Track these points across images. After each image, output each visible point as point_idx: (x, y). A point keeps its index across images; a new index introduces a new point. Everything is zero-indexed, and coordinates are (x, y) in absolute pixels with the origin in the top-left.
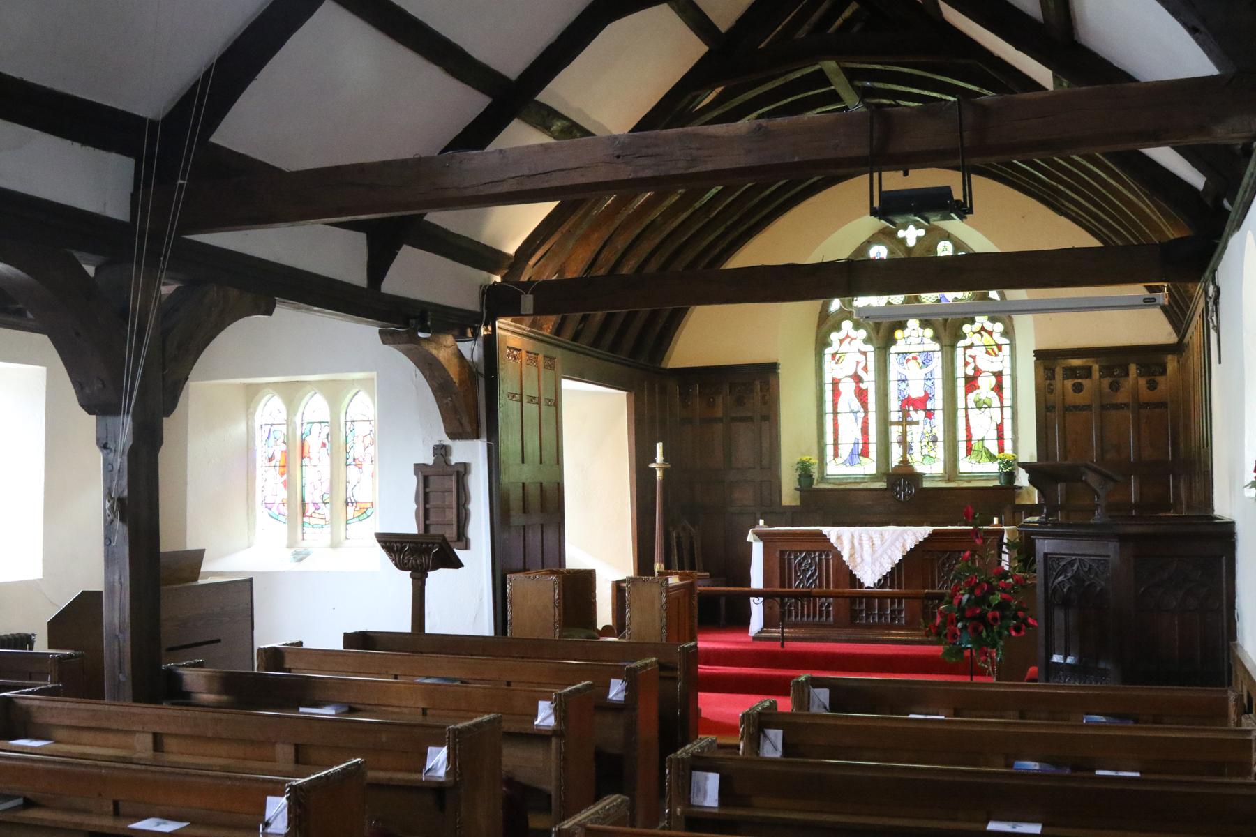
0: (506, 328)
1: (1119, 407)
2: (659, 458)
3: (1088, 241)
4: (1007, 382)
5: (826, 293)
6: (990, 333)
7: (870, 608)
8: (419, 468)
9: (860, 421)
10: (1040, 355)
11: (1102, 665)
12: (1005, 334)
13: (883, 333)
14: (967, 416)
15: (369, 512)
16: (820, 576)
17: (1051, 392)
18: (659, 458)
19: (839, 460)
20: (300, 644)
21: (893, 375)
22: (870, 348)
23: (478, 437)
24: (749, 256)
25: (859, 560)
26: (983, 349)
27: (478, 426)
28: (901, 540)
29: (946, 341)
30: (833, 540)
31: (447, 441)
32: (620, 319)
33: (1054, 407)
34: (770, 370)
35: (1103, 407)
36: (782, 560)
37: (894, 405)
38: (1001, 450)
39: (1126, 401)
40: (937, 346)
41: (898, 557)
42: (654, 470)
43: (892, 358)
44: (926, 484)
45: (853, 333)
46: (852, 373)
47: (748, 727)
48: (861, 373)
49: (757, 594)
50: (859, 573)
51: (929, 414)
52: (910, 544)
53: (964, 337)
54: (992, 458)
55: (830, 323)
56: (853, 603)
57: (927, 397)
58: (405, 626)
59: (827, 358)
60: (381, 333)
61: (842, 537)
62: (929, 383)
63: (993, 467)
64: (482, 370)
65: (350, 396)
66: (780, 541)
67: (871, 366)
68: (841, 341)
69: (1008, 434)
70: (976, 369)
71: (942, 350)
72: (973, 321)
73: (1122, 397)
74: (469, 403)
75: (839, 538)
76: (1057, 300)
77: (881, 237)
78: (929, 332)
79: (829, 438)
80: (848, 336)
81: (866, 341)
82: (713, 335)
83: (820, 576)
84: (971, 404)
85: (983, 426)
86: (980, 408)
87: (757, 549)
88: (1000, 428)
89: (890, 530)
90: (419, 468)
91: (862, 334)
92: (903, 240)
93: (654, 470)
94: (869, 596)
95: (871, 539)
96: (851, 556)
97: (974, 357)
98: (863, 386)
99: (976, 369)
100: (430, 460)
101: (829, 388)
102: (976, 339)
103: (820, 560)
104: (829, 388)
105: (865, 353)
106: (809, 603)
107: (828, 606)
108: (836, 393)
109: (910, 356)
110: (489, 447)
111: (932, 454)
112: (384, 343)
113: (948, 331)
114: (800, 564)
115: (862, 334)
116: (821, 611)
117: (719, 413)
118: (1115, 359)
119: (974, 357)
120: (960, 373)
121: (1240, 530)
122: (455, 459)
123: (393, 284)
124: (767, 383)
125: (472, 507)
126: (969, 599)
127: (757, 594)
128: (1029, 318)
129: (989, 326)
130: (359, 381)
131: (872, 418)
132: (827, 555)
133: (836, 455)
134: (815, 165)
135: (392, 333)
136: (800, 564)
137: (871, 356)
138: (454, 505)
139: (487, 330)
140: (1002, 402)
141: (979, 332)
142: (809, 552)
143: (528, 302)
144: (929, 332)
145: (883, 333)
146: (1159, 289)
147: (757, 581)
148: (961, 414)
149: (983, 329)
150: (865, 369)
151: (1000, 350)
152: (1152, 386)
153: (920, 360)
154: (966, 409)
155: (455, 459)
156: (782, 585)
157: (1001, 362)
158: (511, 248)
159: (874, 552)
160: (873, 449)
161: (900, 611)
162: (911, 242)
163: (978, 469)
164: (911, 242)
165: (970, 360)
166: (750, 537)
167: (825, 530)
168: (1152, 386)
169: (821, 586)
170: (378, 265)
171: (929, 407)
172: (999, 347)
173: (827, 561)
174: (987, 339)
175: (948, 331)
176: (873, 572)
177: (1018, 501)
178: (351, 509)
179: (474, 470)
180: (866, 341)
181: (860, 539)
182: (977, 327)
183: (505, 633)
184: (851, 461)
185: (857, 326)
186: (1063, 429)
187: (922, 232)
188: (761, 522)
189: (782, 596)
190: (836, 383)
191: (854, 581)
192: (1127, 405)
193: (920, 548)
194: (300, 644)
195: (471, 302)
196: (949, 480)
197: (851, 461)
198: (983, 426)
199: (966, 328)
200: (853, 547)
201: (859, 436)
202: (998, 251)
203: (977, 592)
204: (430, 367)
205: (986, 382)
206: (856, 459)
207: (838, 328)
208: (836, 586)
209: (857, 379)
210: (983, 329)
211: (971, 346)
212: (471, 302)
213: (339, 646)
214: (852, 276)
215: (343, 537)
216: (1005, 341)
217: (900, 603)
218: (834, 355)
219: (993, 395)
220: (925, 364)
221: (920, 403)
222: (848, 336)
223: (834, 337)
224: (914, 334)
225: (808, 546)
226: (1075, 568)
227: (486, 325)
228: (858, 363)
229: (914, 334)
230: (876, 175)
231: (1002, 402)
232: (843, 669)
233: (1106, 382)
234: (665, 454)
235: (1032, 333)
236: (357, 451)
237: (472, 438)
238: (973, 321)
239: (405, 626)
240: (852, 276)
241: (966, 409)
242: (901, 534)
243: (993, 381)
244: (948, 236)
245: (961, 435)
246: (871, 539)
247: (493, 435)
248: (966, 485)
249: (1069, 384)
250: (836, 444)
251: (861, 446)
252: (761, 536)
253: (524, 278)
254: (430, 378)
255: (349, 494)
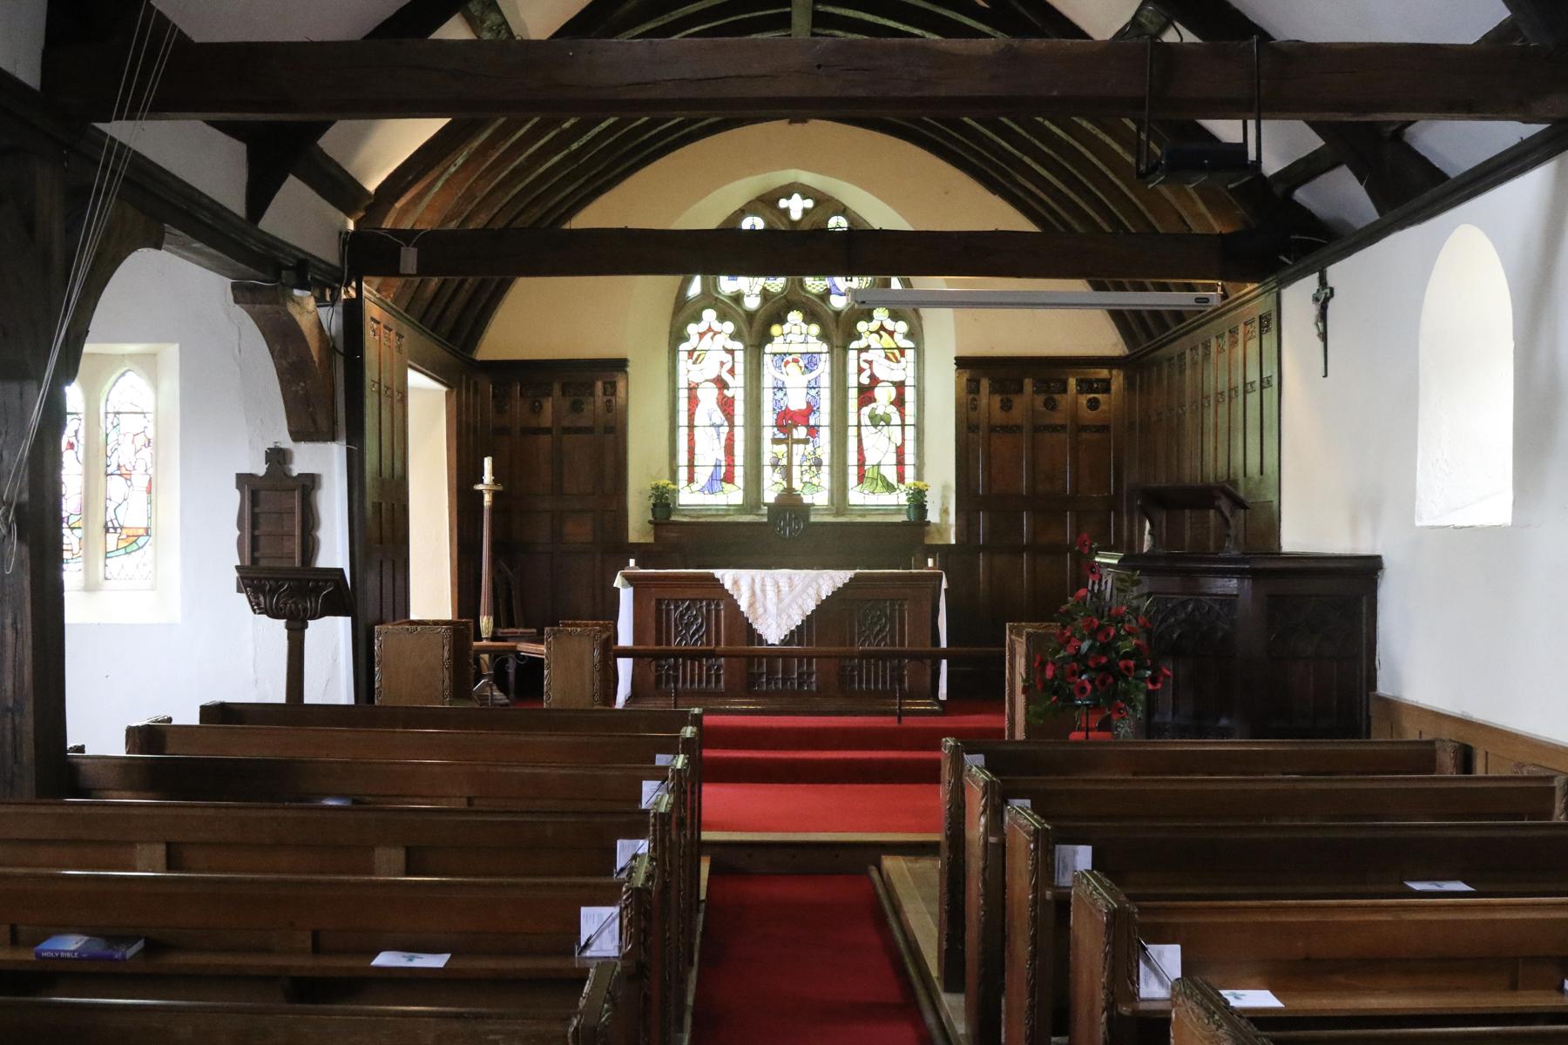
0: (372, 296)
1: (1054, 429)
2: (488, 477)
3: (1020, 223)
4: (910, 394)
5: (686, 270)
6: (891, 334)
7: (771, 672)
8: (243, 480)
9: (723, 437)
10: (962, 363)
11: (1224, 722)
12: (909, 335)
13: (755, 331)
14: (859, 435)
15: (141, 541)
16: (708, 631)
17: (975, 408)
18: (488, 477)
19: (695, 487)
20: (170, 720)
21: (767, 382)
22: (738, 345)
23: (333, 439)
24: (595, 216)
25: (760, 611)
26: (882, 353)
27: (334, 422)
28: (815, 586)
29: (838, 341)
30: (727, 586)
31: (286, 442)
32: (454, 286)
33: (977, 427)
34: (619, 365)
35: (1037, 429)
36: (659, 610)
37: (768, 418)
38: (901, 479)
39: (1061, 422)
40: (825, 347)
41: (811, 606)
42: (481, 493)
43: (767, 359)
44: (813, 519)
45: (716, 326)
46: (714, 376)
47: (993, 798)
48: (727, 377)
49: (625, 653)
50: (760, 627)
51: (813, 431)
52: (826, 591)
53: (859, 337)
54: (890, 488)
55: (688, 311)
56: (750, 664)
57: (811, 409)
58: (278, 695)
59: (683, 356)
60: (234, 287)
61: (739, 582)
62: (813, 392)
63: (901, 498)
64: (340, 346)
65: (114, 378)
66: (656, 586)
67: (740, 369)
68: (702, 335)
69: (910, 458)
70: (873, 377)
71: (831, 352)
72: (870, 318)
73: (1058, 418)
74: (329, 392)
75: (735, 583)
76: (1057, 294)
77: (760, 206)
78: (815, 329)
79: (683, 458)
80: (710, 329)
81: (733, 337)
82: (541, 318)
83: (708, 631)
84: (865, 420)
85: (879, 447)
86: (875, 426)
87: (626, 596)
88: (900, 451)
89: (800, 576)
90: (243, 480)
91: (729, 327)
92: (786, 211)
93: (481, 493)
94: (773, 655)
95: (777, 584)
96: (751, 605)
97: (870, 363)
98: (728, 393)
99: (873, 377)
100: (260, 469)
101: (683, 395)
102: (873, 340)
103: (708, 611)
104: (683, 395)
105: (731, 352)
106: (693, 665)
107: (718, 669)
108: (693, 401)
109: (789, 358)
110: (350, 453)
111: (815, 481)
112: (236, 301)
113: (840, 331)
114: (682, 615)
115: (729, 327)
116: (709, 676)
117: (546, 419)
118: (1048, 371)
119: (870, 363)
120: (852, 381)
121: (1386, 562)
122: (297, 468)
123: (270, 223)
124: (614, 385)
125: (323, 534)
126: (1091, 648)
127: (625, 653)
128: (948, 313)
129: (889, 325)
130: (131, 356)
131: (739, 434)
132: (718, 605)
133: (691, 479)
134: (710, 104)
135: (253, 289)
136: (682, 615)
137: (740, 356)
138: (297, 532)
139: (347, 292)
140: (903, 420)
141: (877, 332)
142: (693, 601)
143: (409, 258)
144: (815, 329)
145: (755, 331)
146: (1212, 288)
147: (625, 638)
148: (852, 432)
149: (882, 328)
150: (732, 371)
151: (902, 355)
152: (1006, 406)
153: (802, 363)
154: (859, 426)
155: (297, 468)
156: (659, 643)
157: (905, 370)
158: (372, 186)
159: (780, 600)
160: (739, 472)
161: (810, 675)
162: (796, 215)
163: (874, 501)
164: (796, 215)
165: (865, 366)
166: (618, 582)
167: (718, 573)
168: (1051, 405)
169: (709, 643)
170: (260, 193)
171: (812, 422)
172: (902, 351)
173: (718, 612)
174: (886, 341)
175: (840, 331)
176: (779, 626)
177: (928, 541)
178: (112, 538)
179: (325, 482)
180: (733, 337)
181: (763, 585)
182: (875, 325)
183: (371, 699)
184: (710, 488)
185: (722, 318)
186: (989, 457)
187: (809, 204)
188: (632, 562)
189: (657, 656)
190: (692, 389)
191: (752, 635)
192: (1063, 427)
193: (839, 595)
194: (170, 720)
195: (328, 252)
196: (838, 514)
197: (710, 488)
198: (879, 447)
199: (862, 326)
200: (753, 594)
201: (722, 456)
202: (911, 229)
203: (1101, 637)
204: (282, 336)
205: (884, 394)
206: (717, 486)
207: (697, 319)
208: (728, 643)
209: (721, 384)
210: (882, 328)
211: (868, 348)
212: (328, 252)
213: (194, 719)
214: (722, 250)
215: (101, 576)
216: (908, 344)
217: (810, 664)
218: (691, 353)
219: (892, 410)
220: (809, 368)
221: (803, 417)
222: (710, 329)
223: (692, 329)
224: (796, 330)
225: (691, 593)
226: (1190, 607)
227: (348, 284)
228: (722, 364)
229: (796, 330)
230: (1251, 124)
231: (903, 420)
232: (726, 746)
233: (1040, 399)
234: (494, 473)
235: (949, 335)
236: (123, 454)
237: (325, 440)
238: (870, 318)
239: (278, 695)
240: (722, 250)
241: (859, 426)
242: (815, 579)
243: (893, 393)
244: (843, 211)
245: (852, 458)
246: (777, 584)
247: (355, 436)
248: (859, 520)
249: (1083, 400)
250: (691, 466)
251: (723, 470)
252: (631, 580)
253: (388, 224)
254: (278, 353)
255: (111, 515)
